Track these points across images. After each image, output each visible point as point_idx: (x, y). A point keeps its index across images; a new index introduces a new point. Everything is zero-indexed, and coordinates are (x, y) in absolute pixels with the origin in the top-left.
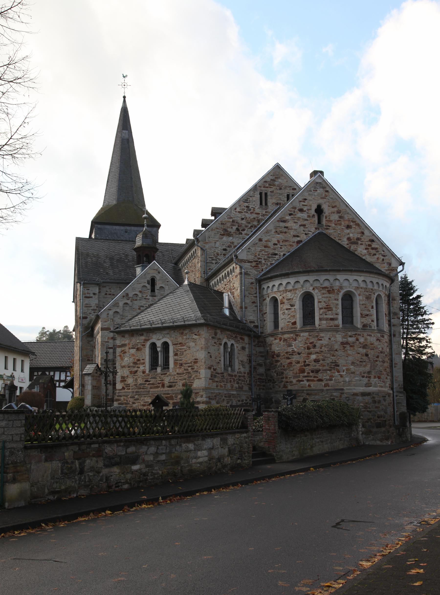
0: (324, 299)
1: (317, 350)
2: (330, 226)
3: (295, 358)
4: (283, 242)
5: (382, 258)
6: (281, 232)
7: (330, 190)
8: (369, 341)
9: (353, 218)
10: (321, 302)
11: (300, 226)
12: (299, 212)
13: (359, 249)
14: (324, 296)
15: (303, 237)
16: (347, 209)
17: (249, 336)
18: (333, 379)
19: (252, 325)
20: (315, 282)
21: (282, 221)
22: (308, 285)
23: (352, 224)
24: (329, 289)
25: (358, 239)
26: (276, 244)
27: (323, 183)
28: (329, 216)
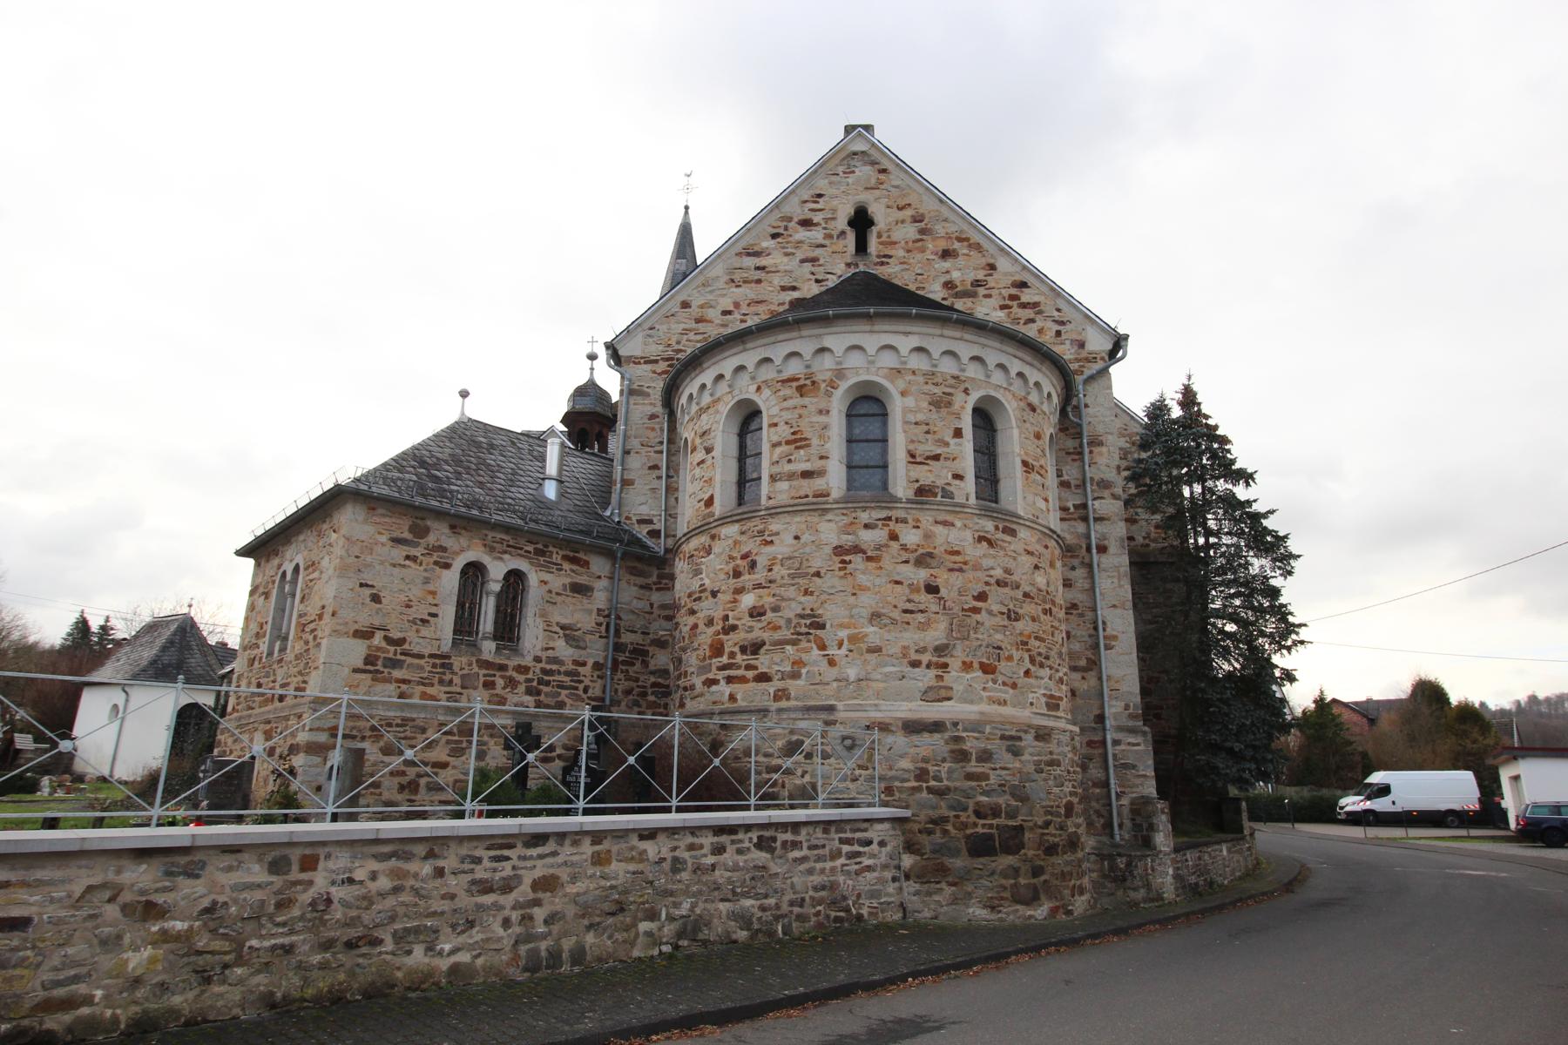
0: (787, 415)
1: (760, 575)
3: (707, 607)
10: (776, 425)
13: (979, 309)
14: (785, 404)
16: (944, 210)
17: (609, 554)
18: (804, 671)
19: (645, 529)
20: (764, 368)
21: (749, 254)
22: (744, 379)
23: (957, 245)
24: (802, 382)
25: (977, 283)
27: (873, 152)
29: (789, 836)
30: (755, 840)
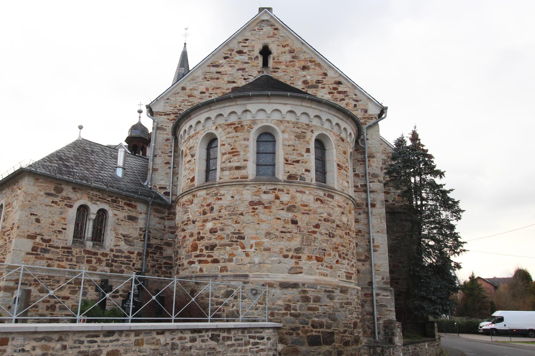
0: (229, 141)
1: (215, 214)
2: (279, 69)
3: (190, 228)
4: (213, 89)
5: (355, 103)
6: (211, 79)
7: (280, 27)
8: (298, 200)
9: (312, 58)
10: (224, 145)
11: (238, 70)
12: (237, 55)
13: (319, 94)
15: (241, 83)
17: (146, 203)
18: (234, 258)
19: (162, 191)
21: (213, 66)
22: (210, 123)
23: (309, 64)
24: (236, 125)
25: (318, 82)
26: (204, 93)
27: (272, 20)
28: (278, 56)
29: (226, 335)
30: (210, 336)
